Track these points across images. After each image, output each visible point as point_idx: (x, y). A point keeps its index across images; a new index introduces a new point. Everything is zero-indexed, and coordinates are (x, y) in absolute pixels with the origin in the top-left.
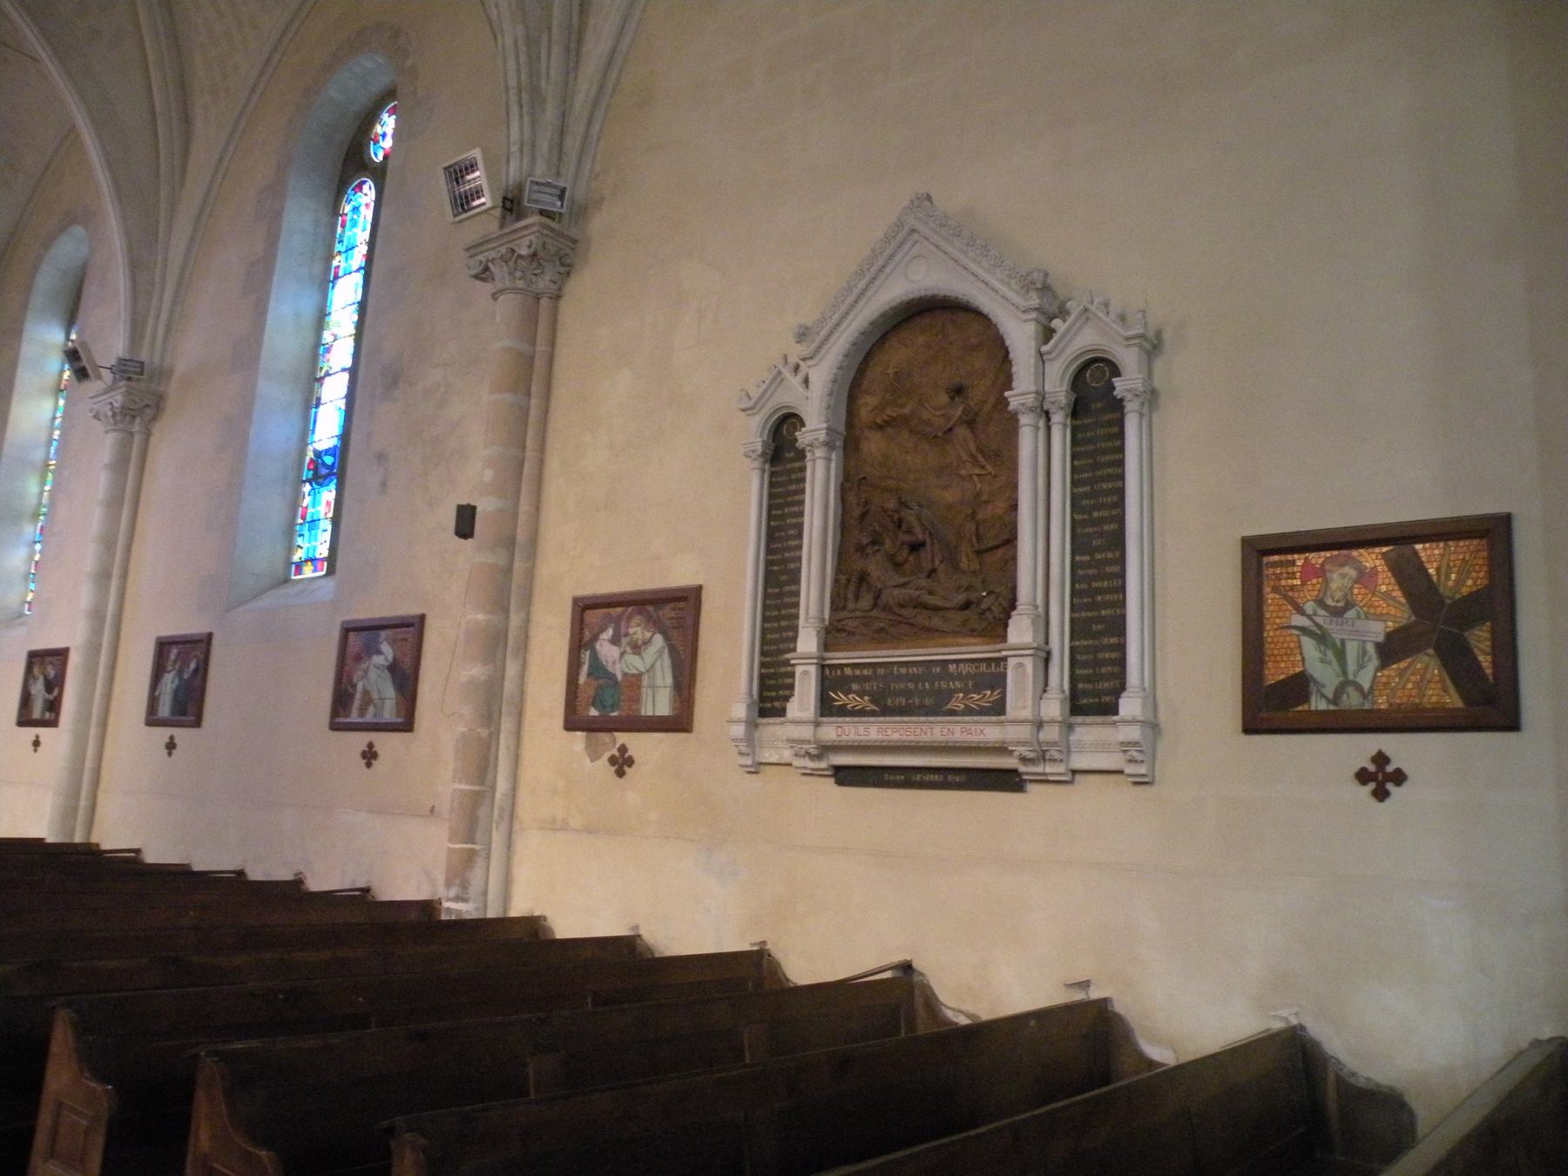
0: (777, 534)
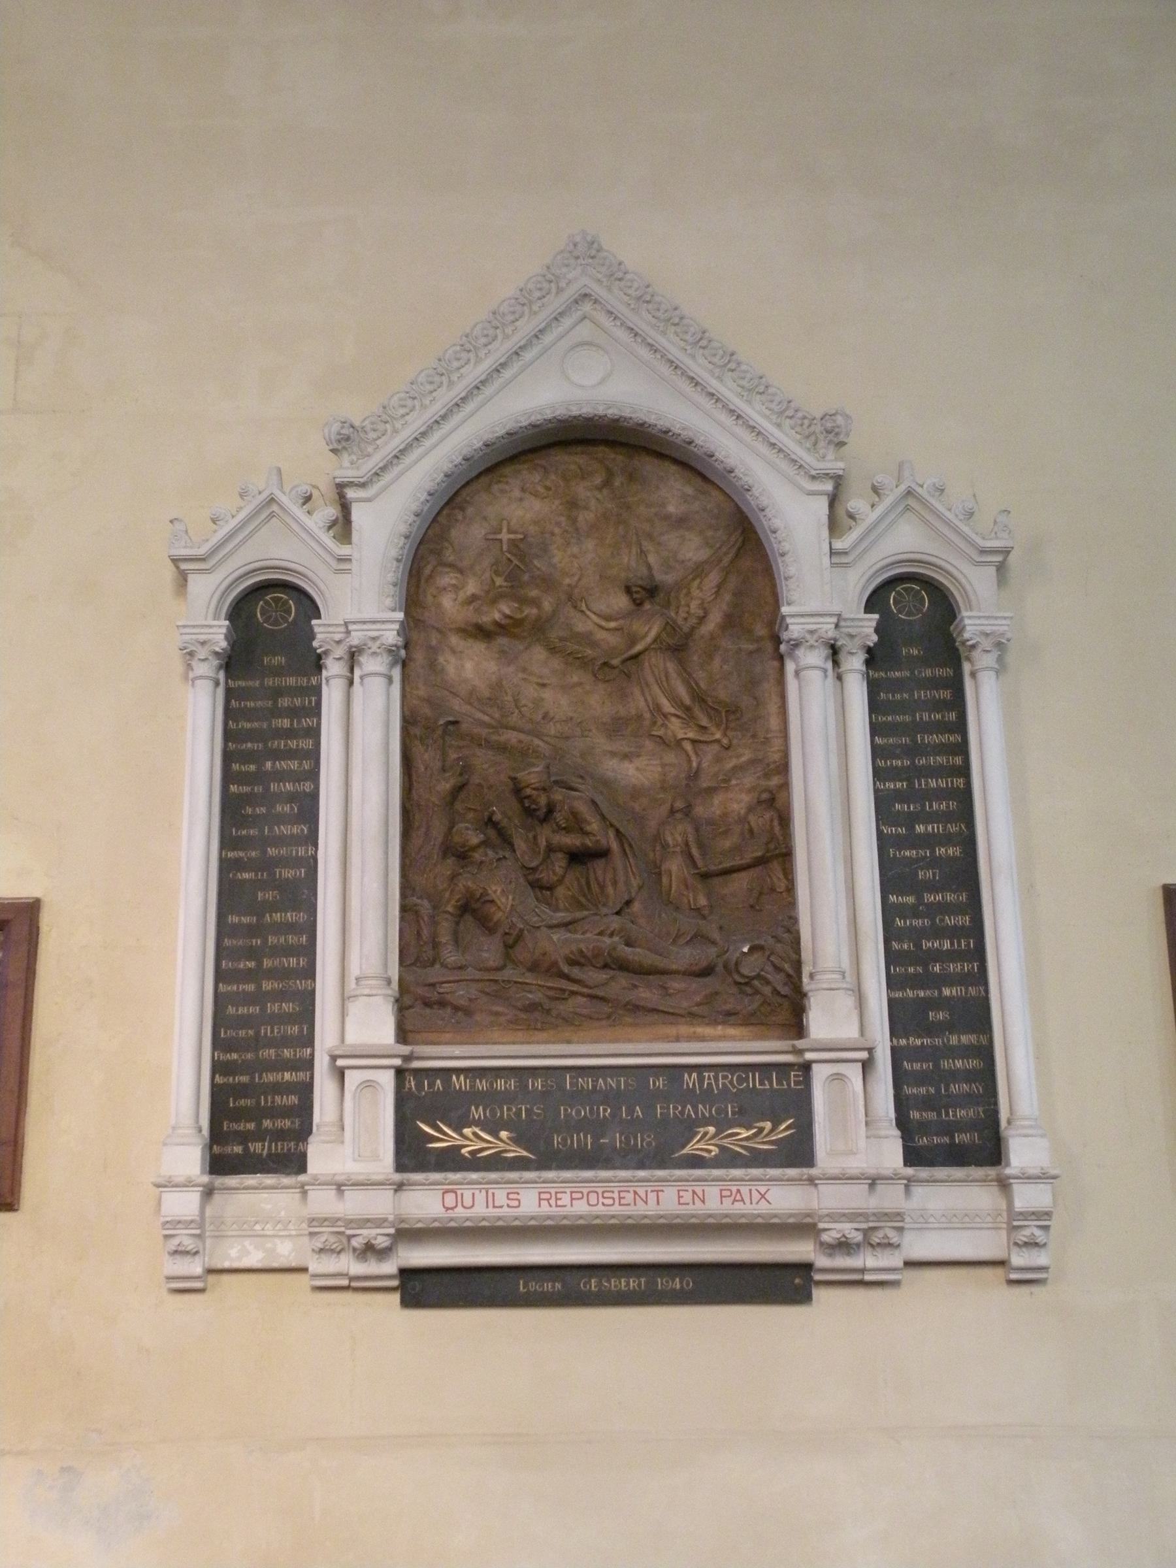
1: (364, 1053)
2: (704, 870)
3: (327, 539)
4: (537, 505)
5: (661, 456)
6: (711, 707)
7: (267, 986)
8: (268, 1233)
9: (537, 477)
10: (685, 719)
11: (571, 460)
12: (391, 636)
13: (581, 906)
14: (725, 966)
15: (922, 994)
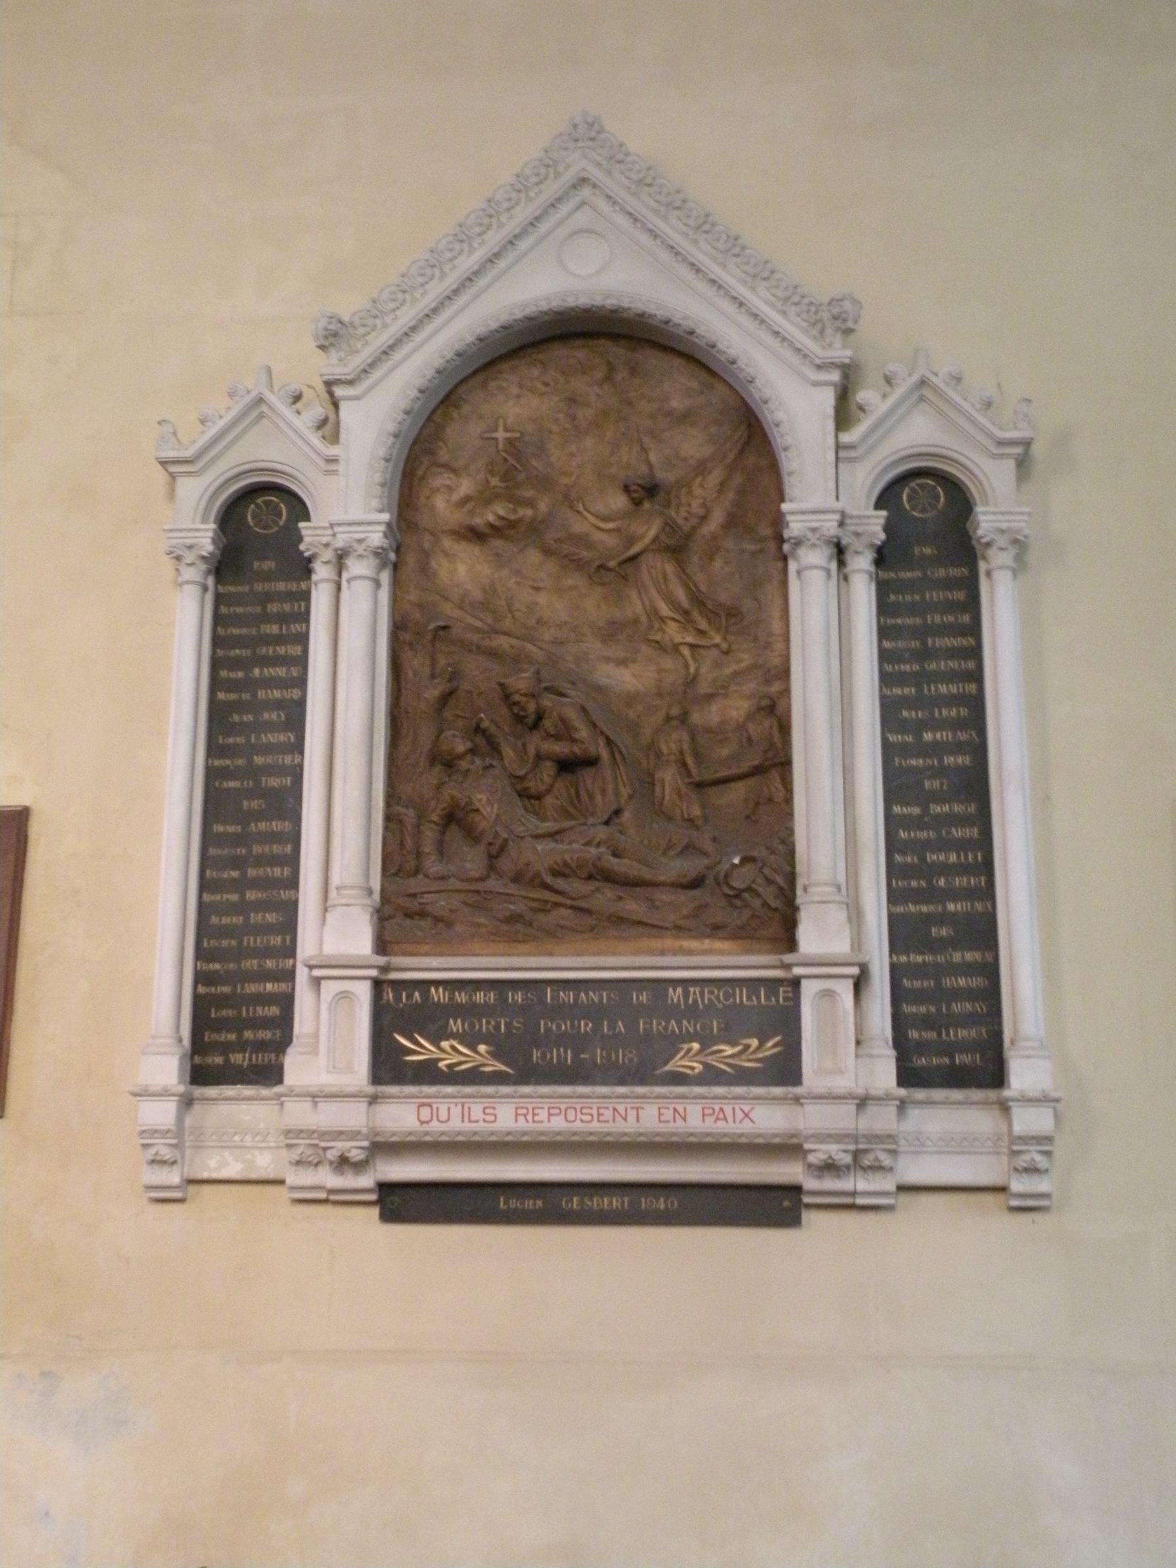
0: (236, 718)
1: (350, 963)
2: (697, 779)
3: (315, 439)
4: (535, 401)
5: (666, 349)
6: (710, 610)
7: (251, 895)
8: (248, 1144)
9: (536, 372)
10: (682, 623)
11: (577, 353)
12: (376, 538)
13: (569, 816)
14: (716, 878)
15: (924, 909)
